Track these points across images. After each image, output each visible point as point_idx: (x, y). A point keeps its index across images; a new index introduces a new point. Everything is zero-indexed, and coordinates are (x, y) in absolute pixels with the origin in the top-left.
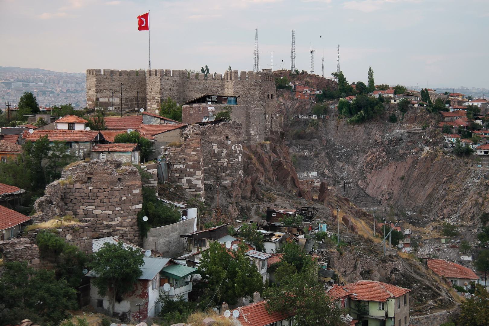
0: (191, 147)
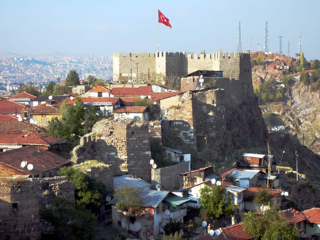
0: (186, 109)
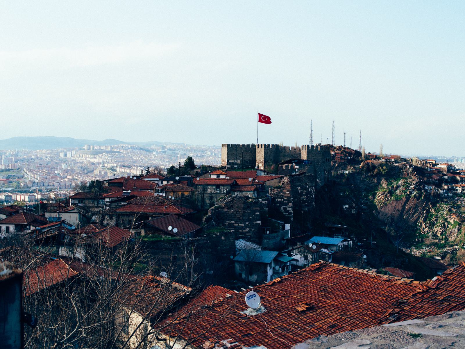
0: (286, 189)
